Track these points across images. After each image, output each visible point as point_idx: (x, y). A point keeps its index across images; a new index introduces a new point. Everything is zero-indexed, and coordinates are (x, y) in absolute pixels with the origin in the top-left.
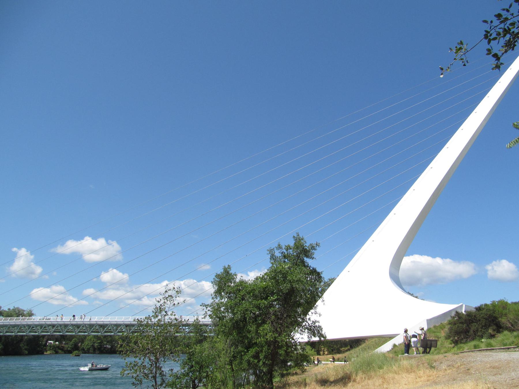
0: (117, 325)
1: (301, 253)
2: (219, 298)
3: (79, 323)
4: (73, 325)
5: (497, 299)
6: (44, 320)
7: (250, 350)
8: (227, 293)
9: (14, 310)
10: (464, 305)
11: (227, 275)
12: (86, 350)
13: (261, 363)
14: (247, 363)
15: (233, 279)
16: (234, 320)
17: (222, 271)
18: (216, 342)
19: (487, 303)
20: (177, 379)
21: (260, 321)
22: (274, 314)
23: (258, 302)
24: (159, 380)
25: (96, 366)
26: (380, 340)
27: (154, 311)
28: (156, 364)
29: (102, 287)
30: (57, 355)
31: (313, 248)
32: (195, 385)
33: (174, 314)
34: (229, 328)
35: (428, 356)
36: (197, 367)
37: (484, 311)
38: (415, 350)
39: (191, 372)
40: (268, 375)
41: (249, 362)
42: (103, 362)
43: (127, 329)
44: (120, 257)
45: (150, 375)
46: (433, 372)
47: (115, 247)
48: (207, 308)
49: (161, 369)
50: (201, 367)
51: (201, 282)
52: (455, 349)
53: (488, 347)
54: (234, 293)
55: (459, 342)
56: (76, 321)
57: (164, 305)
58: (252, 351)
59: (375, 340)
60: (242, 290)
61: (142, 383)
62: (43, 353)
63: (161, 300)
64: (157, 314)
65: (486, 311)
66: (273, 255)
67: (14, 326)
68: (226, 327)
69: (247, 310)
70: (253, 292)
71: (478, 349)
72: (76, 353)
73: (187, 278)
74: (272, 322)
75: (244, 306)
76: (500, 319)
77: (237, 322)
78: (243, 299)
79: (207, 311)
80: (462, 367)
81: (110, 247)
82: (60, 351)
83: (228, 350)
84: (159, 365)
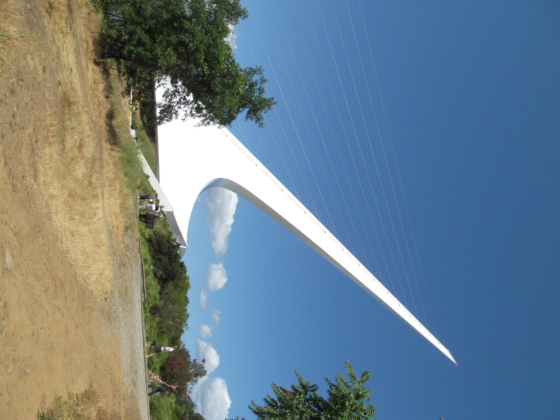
1: (254, 105)
5: (191, 281)
10: (186, 247)
13: (132, 48)
17: (242, 7)
19: (187, 273)
21: (181, 50)
26: (154, 158)
31: (258, 119)
35: (137, 220)
37: (179, 270)
38: (143, 207)
46: (121, 231)
52: (144, 240)
53: (145, 272)
55: (150, 244)
58: (146, 38)
59: (153, 154)
65: (180, 272)
69: (194, 36)
71: (143, 263)
75: (199, 34)
76: (171, 283)
80: (127, 259)
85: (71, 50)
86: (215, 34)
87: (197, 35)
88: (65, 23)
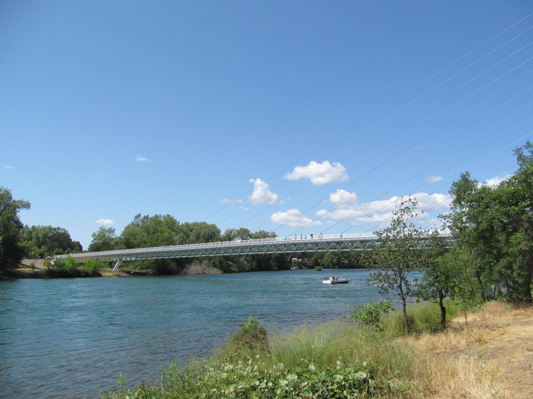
0: (353, 242)
2: (458, 208)
3: (317, 241)
4: (312, 243)
6: (287, 240)
7: (500, 260)
8: (468, 201)
9: (260, 232)
11: (466, 183)
12: (326, 265)
13: (515, 274)
14: (499, 273)
15: (474, 186)
16: (480, 229)
17: (460, 178)
18: (459, 254)
20: (422, 289)
21: (510, 229)
22: (527, 221)
23: (507, 209)
24: (404, 288)
25: (337, 280)
27: (392, 223)
28: (400, 275)
29: (333, 207)
30: (301, 270)
32: (442, 295)
33: (412, 225)
34: (473, 238)
36: (443, 278)
39: (436, 282)
40: (525, 286)
41: (500, 273)
42: (342, 275)
43: (362, 245)
44: (345, 178)
45: (395, 286)
47: (340, 168)
48: (445, 219)
49: (405, 279)
50: (447, 278)
51: (432, 195)
54: (476, 201)
56: (314, 240)
57: (402, 217)
58: (503, 262)
60: (486, 198)
61: (388, 292)
62: (289, 269)
63: (398, 212)
64: (395, 226)
66: (521, 155)
67: (263, 246)
68: (470, 237)
69: (493, 218)
70: (499, 198)
72: (318, 268)
73: (416, 192)
74: (525, 230)
75: (490, 214)
77: (483, 231)
78: (487, 207)
79: (445, 222)
81: (334, 168)
82: (303, 267)
83: (474, 261)
84: (403, 275)
85: (522, 328)
86: (488, 199)
87: (492, 215)
88: (495, 332)
